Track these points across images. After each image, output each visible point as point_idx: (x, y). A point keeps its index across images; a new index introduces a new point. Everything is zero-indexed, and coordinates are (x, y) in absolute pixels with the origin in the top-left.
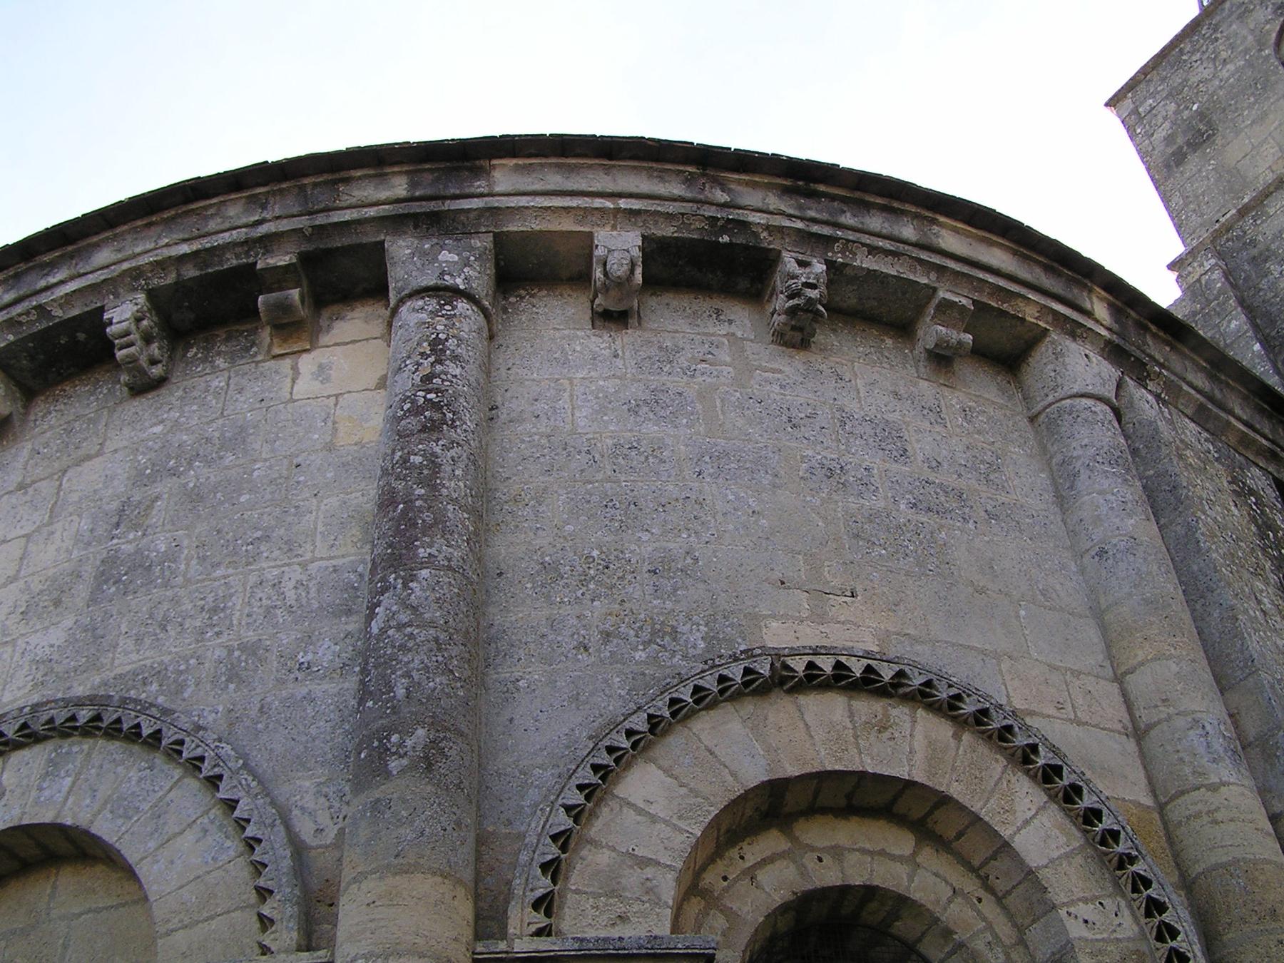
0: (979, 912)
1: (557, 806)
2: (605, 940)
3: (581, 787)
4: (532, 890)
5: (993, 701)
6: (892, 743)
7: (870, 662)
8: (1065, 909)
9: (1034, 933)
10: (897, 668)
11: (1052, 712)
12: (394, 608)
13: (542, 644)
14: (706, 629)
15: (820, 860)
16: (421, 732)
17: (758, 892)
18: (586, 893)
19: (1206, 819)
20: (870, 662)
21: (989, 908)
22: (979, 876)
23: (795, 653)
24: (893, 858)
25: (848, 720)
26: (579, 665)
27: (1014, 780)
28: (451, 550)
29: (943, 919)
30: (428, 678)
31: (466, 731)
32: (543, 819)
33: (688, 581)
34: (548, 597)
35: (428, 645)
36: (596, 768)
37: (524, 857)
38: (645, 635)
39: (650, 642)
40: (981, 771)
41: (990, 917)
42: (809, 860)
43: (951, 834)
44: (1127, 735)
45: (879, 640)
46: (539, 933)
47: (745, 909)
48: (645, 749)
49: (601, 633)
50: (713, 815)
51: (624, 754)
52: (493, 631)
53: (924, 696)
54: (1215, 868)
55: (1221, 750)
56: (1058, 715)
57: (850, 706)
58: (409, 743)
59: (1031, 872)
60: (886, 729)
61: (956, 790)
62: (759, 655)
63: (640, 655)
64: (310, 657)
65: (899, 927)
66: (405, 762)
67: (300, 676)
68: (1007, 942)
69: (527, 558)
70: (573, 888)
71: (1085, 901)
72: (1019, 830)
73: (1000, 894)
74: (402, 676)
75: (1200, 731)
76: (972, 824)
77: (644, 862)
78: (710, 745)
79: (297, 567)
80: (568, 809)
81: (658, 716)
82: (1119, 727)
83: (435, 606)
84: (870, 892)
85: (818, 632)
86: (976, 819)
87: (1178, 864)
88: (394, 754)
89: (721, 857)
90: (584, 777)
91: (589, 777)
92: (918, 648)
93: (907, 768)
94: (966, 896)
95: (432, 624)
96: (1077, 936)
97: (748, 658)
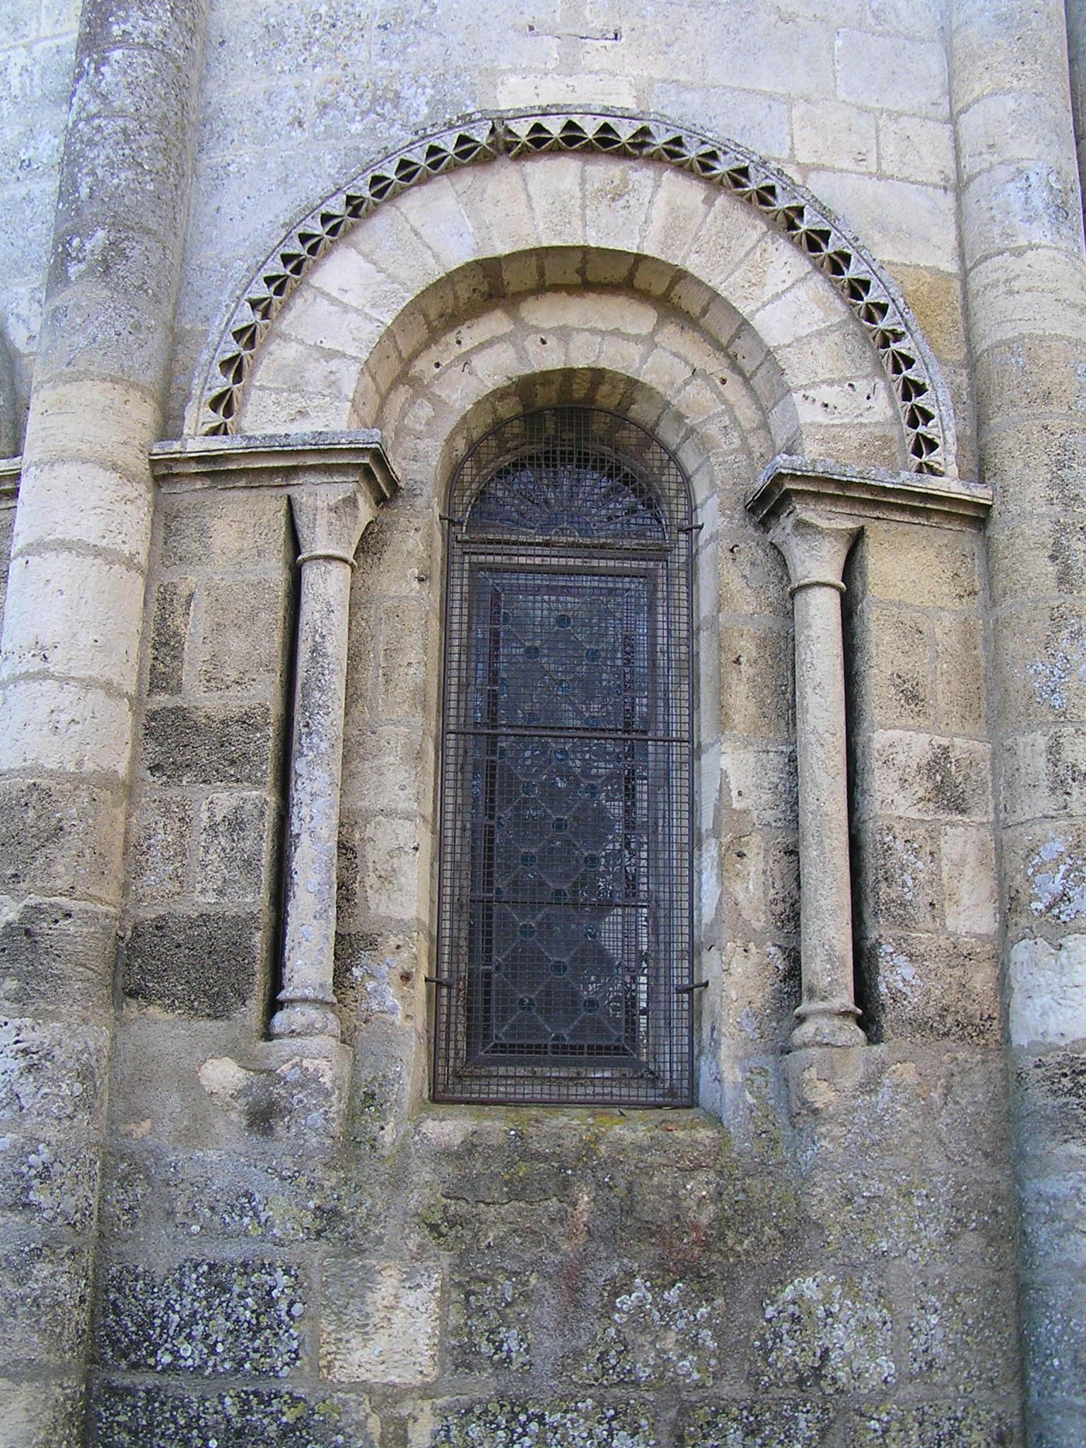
0: (720, 394)
1: (243, 301)
2: (272, 437)
3: (269, 281)
4: (210, 389)
5: (754, 158)
6: (625, 212)
7: (608, 120)
8: (802, 392)
9: (775, 417)
10: (638, 125)
11: (848, 164)
12: (85, 98)
13: (257, 122)
14: (432, 92)
15: (544, 342)
16: (101, 234)
17: (471, 378)
18: (269, 389)
19: (1002, 288)
20: (608, 120)
21: (734, 390)
22: (727, 356)
23: (520, 115)
24: (627, 337)
25: (577, 188)
26: (291, 143)
27: (771, 248)
28: (147, 24)
29: (675, 402)
30: (112, 174)
31: (155, 227)
32: (228, 316)
33: (421, 35)
34: (268, 66)
35: (116, 138)
36: (286, 259)
37: (205, 357)
38: (365, 104)
39: (369, 110)
40: (730, 239)
41: (732, 399)
42: (532, 343)
43: (696, 310)
44: (945, 189)
45: (638, 91)
46: (214, 432)
47: (455, 397)
48: (346, 233)
49: (318, 104)
50: (408, 301)
51: (319, 241)
52: (210, 110)
53: (672, 155)
54: (1001, 343)
55: (1041, 206)
56: (858, 169)
57: (583, 171)
58: (88, 246)
59: (769, 353)
60: (621, 196)
61: (693, 264)
62: (480, 120)
63: (356, 128)
64: (31, 153)
65: (637, 411)
66: (83, 267)
67: (21, 174)
68: (746, 425)
69: (251, 21)
70: (258, 384)
71: (831, 383)
72: (764, 305)
73: (748, 375)
74: (87, 174)
75: (1023, 184)
76: (711, 300)
77: (331, 355)
78: (417, 225)
79: (22, 50)
80: (254, 304)
81: (358, 198)
82: (937, 179)
83: (126, 92)
84: (597, 376)
85: (564, 86)
86: (715, 295)
87: (968, 339)
88: (74, 259)
89: (436, 342)
90: (272, 269)
91: (276, 268)
92: (687, 96)
93: (637, 241)
94: (707, 377)
95: (122, 113)
96: (809, 421)
97: (465, 124)
